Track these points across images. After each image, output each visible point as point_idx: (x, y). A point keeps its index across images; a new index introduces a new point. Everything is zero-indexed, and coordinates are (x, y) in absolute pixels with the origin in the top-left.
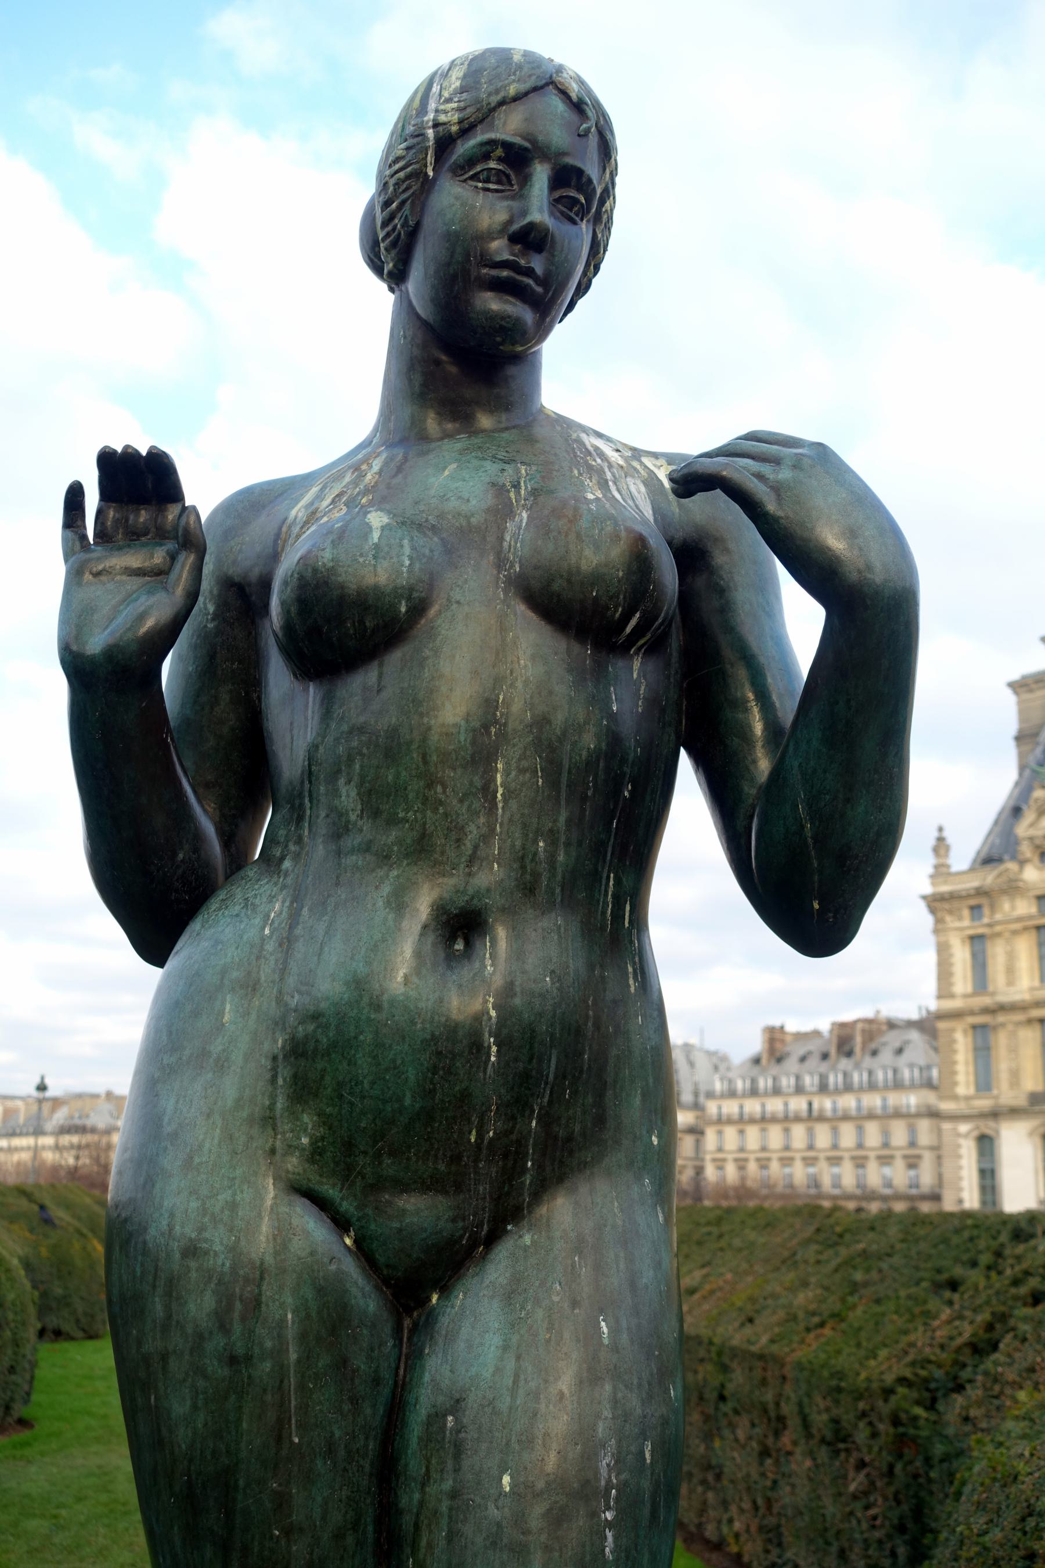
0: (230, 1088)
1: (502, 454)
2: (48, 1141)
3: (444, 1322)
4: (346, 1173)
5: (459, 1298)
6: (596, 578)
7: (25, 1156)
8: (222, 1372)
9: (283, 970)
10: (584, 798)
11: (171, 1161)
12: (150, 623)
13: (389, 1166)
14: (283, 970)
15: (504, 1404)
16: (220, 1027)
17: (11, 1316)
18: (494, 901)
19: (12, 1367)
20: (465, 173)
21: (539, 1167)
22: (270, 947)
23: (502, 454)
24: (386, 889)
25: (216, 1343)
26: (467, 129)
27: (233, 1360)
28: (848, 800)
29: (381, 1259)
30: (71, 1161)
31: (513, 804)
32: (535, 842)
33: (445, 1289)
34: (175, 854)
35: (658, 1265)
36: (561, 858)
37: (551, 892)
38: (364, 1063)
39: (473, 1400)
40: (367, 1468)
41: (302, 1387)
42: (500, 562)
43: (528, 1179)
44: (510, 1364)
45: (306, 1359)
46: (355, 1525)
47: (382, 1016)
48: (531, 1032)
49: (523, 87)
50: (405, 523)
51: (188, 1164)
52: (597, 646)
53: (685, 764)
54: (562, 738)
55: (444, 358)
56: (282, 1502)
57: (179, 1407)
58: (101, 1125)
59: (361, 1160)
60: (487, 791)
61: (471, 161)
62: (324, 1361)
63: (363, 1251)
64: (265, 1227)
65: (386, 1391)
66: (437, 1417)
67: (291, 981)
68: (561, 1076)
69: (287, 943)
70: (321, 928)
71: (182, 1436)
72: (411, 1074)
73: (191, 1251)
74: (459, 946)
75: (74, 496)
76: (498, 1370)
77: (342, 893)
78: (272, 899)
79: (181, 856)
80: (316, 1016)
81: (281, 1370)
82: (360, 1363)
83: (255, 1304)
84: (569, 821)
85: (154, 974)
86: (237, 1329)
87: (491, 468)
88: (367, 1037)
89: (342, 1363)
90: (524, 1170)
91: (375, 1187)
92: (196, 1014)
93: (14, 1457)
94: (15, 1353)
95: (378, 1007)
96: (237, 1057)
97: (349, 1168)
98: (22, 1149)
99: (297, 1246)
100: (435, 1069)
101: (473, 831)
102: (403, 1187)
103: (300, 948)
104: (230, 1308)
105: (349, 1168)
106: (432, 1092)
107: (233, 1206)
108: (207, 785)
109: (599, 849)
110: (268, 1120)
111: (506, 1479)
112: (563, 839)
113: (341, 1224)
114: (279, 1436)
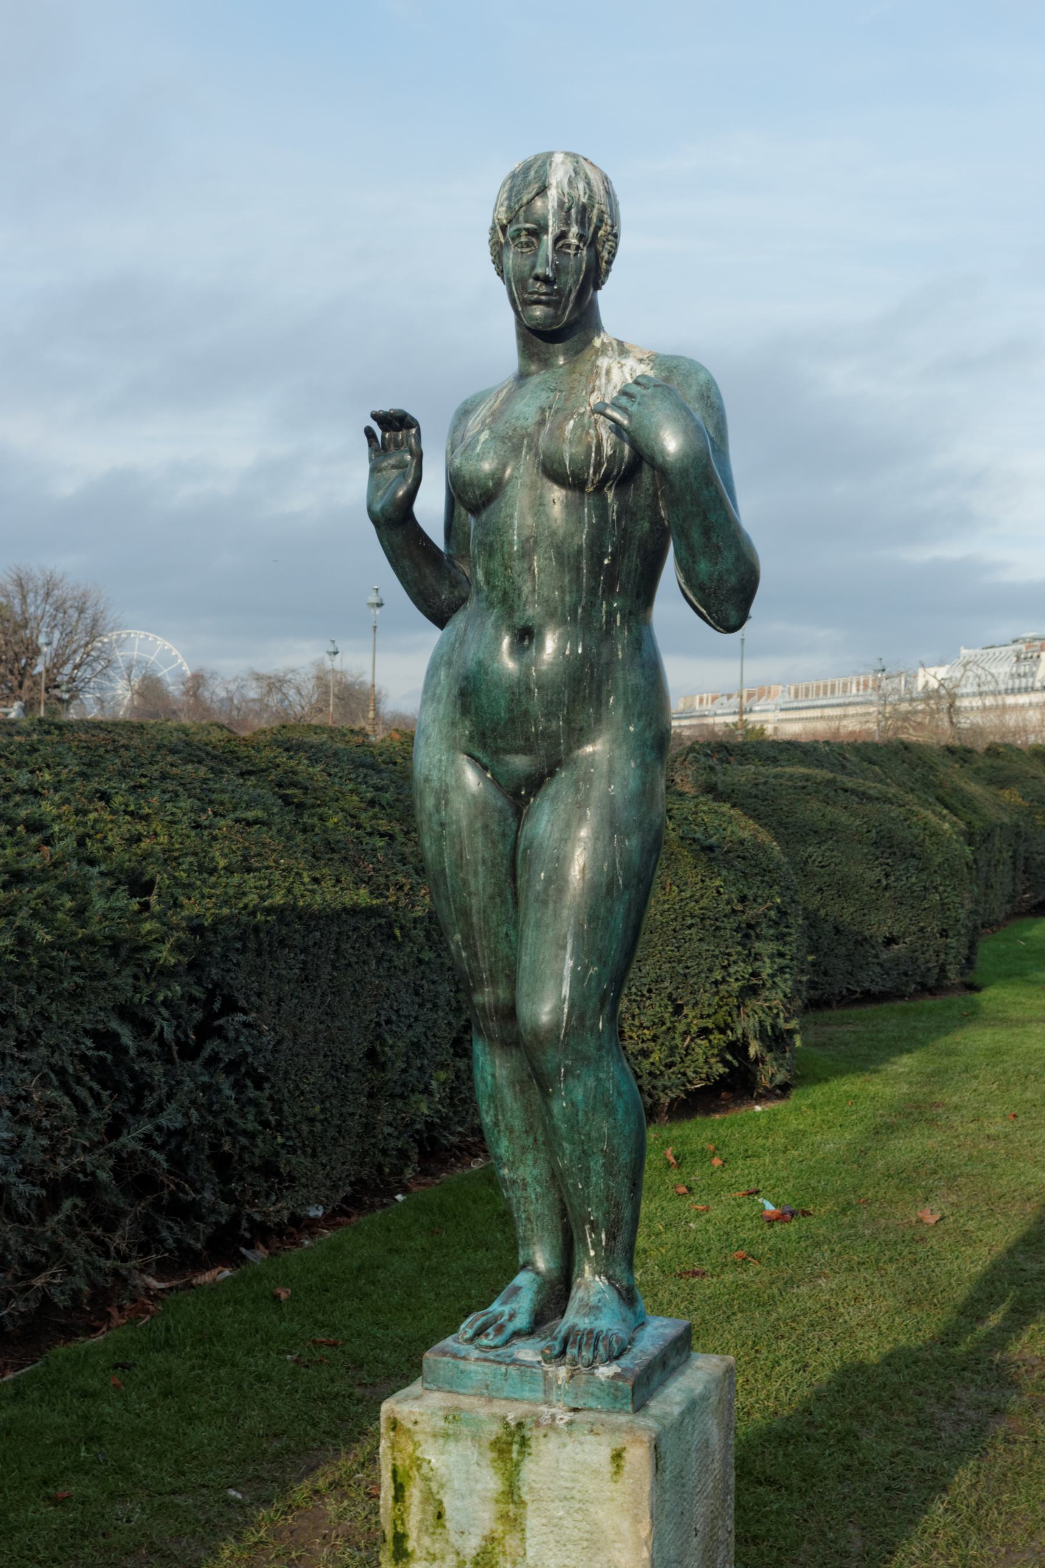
4: (484, 747)
8: (438, 829)
12: (401, 493)
13: (500, 743)
15: (545, 845)
25: (435, 818)
28: (694, 562)
31: (542, 575)
32: (553, 592)
34: (440, 597)
36: (567, 598)
38: (483, 698)
39: (536, 842)
40: (504, 871)
42: (536, 455)
43: (562, 748)
44: (549, 828)
45: (471, 824)
47: (489, 677)
59: (489, 741)
60: (530, 569)
65: (511, 840)
72: (503, 703)
75: (369, 433)
79: (443, 597)
84: (570, 581)
91: (496, 752)
95: (487, 674)
96: (444, 695)
97: (485, 744)
105: (485, 744)
106: (512, 710)
111: (542, 875)
112: (568, 589)
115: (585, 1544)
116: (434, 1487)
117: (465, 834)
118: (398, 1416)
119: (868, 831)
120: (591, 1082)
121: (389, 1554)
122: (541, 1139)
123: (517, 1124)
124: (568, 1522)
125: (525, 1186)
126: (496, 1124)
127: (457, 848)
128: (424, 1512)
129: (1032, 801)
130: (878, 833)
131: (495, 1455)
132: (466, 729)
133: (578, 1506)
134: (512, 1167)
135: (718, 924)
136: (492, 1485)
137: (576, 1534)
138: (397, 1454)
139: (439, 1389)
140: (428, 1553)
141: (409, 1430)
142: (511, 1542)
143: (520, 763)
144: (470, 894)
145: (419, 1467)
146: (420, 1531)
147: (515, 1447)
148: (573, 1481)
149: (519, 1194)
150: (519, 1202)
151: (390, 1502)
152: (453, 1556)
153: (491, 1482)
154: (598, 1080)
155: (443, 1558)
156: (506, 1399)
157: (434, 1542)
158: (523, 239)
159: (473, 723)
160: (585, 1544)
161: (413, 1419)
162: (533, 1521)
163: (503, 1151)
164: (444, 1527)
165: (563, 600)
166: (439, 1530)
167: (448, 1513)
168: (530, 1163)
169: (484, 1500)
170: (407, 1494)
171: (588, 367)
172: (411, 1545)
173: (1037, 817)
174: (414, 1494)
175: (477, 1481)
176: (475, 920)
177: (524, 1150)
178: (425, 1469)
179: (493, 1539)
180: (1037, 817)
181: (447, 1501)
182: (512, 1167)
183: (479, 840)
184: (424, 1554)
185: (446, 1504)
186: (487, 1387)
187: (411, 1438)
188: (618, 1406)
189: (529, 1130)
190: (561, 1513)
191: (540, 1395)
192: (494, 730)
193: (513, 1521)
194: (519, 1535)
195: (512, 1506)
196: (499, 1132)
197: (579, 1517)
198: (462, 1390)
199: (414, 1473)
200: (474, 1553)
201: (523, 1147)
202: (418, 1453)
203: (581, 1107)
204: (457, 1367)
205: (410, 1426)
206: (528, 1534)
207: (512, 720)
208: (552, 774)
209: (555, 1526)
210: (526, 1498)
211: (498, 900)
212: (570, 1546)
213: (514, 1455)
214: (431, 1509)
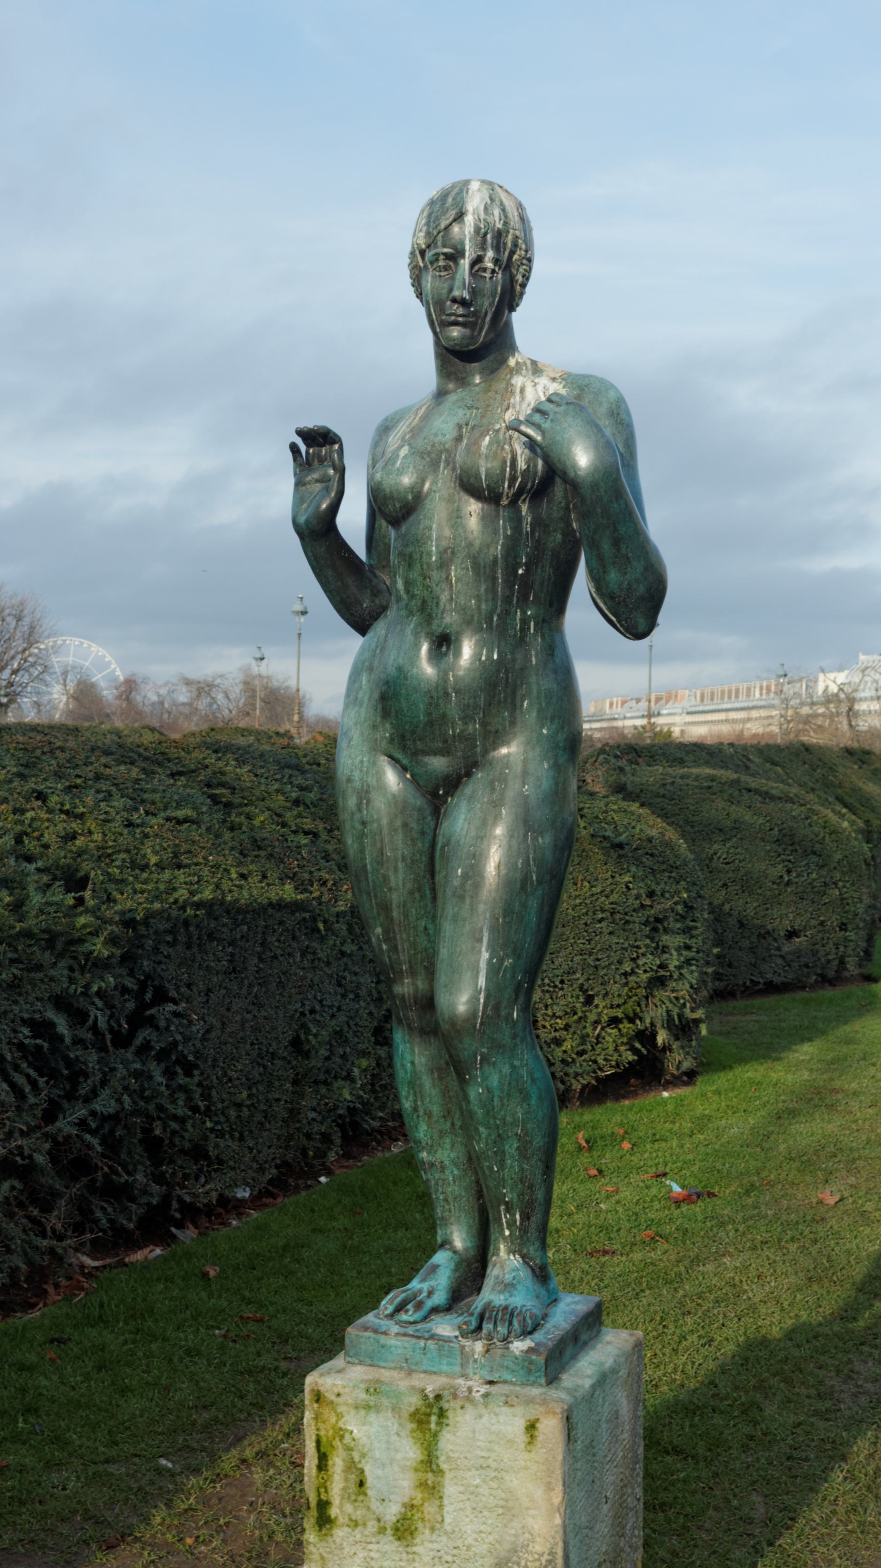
4: (404, 748)
12: (324, 506)
25: (357, 816)
36: (484, 607)
37: (480, 623)
38: (403, 701)
39: (453, 840)
40: (423, 867)
42: (454, 469)
43: (478, 749)
44: (466, 826)
45: (391, 822)
46: (419, 890)
54: (480, 552)
55: (333, 494)
60: (448, 578)
65: (429, 838)
75: (294, 448)
76: (462, 829)
84: (486, 590)
85: (355, 642)
90: (476, 746)
91: (415, 754)
95: (406, 679)
96: (366, 699)
100: (431, 704)
102: (426, 753)
106: (431, 714)
115: (500, 1511)
116: (356, 1456)
118: (322, 1389)
120: (506, 1070)
121: (313, 1521)
122: (458, 1124)
123: (435, 1109)
124: (484, 1490)
125: (443, 1169)
126: (415, 1109)
128: (346, 1480)
130: (780, 831)
131: (414, 1426)
132: (386, 731)
133: (493, 1474)
134: (431, 1150)
135: (627, 918)
139: (361, 1363)
140: (351, 1520)
141: (332, 1402)
142: (430, 1509)
143: (438, 764)
145: (342, 1437)
147: (434, 1418)
148: (489, 1450)
149: (437, 1176)
150: (437, 1184)
152: (375, 1523)
155: (365, 1524)
156: (425, 1372)
157: (356, 1508)
159: (393, 726)
160: (500, 1511)
161: (336, 1391)
162: (450, 1489)
163: (422, 1135)
164: (365, 1494)
166: (361, 1498)
167: (370, 1481)
168: (448, 1146)
170: (330, 1463)
171: (503, 385)
172: (334, 1512)
174: (337, 1463)
175: (397, 1451)
176: (395, 914)
177: (442, 1134)
178: (347, 1439)
182: (431, 1150)
184: (346, 1520)
185: (367, 1473)
186: (407, 1360)
188: (532, 1378)
189: (447, 1115)
190: (477, 1481)
192: (413, 732)
194: (437, 1502)
195: (430, 1475)
196: (418, 1117)
197: (494, 1485)
198: (382, 1364)
199: (337, 1443)
200: (394, 1519)
202: (341, 1424)
203: (497, 1093)
204: (378, 1342)
205: (333, 1398)
206: (446, 1501)
208: (469, 774)
210: (444, 1466)
212: (486, 1513)
213: (433, 1426)
214: (353, 1477)
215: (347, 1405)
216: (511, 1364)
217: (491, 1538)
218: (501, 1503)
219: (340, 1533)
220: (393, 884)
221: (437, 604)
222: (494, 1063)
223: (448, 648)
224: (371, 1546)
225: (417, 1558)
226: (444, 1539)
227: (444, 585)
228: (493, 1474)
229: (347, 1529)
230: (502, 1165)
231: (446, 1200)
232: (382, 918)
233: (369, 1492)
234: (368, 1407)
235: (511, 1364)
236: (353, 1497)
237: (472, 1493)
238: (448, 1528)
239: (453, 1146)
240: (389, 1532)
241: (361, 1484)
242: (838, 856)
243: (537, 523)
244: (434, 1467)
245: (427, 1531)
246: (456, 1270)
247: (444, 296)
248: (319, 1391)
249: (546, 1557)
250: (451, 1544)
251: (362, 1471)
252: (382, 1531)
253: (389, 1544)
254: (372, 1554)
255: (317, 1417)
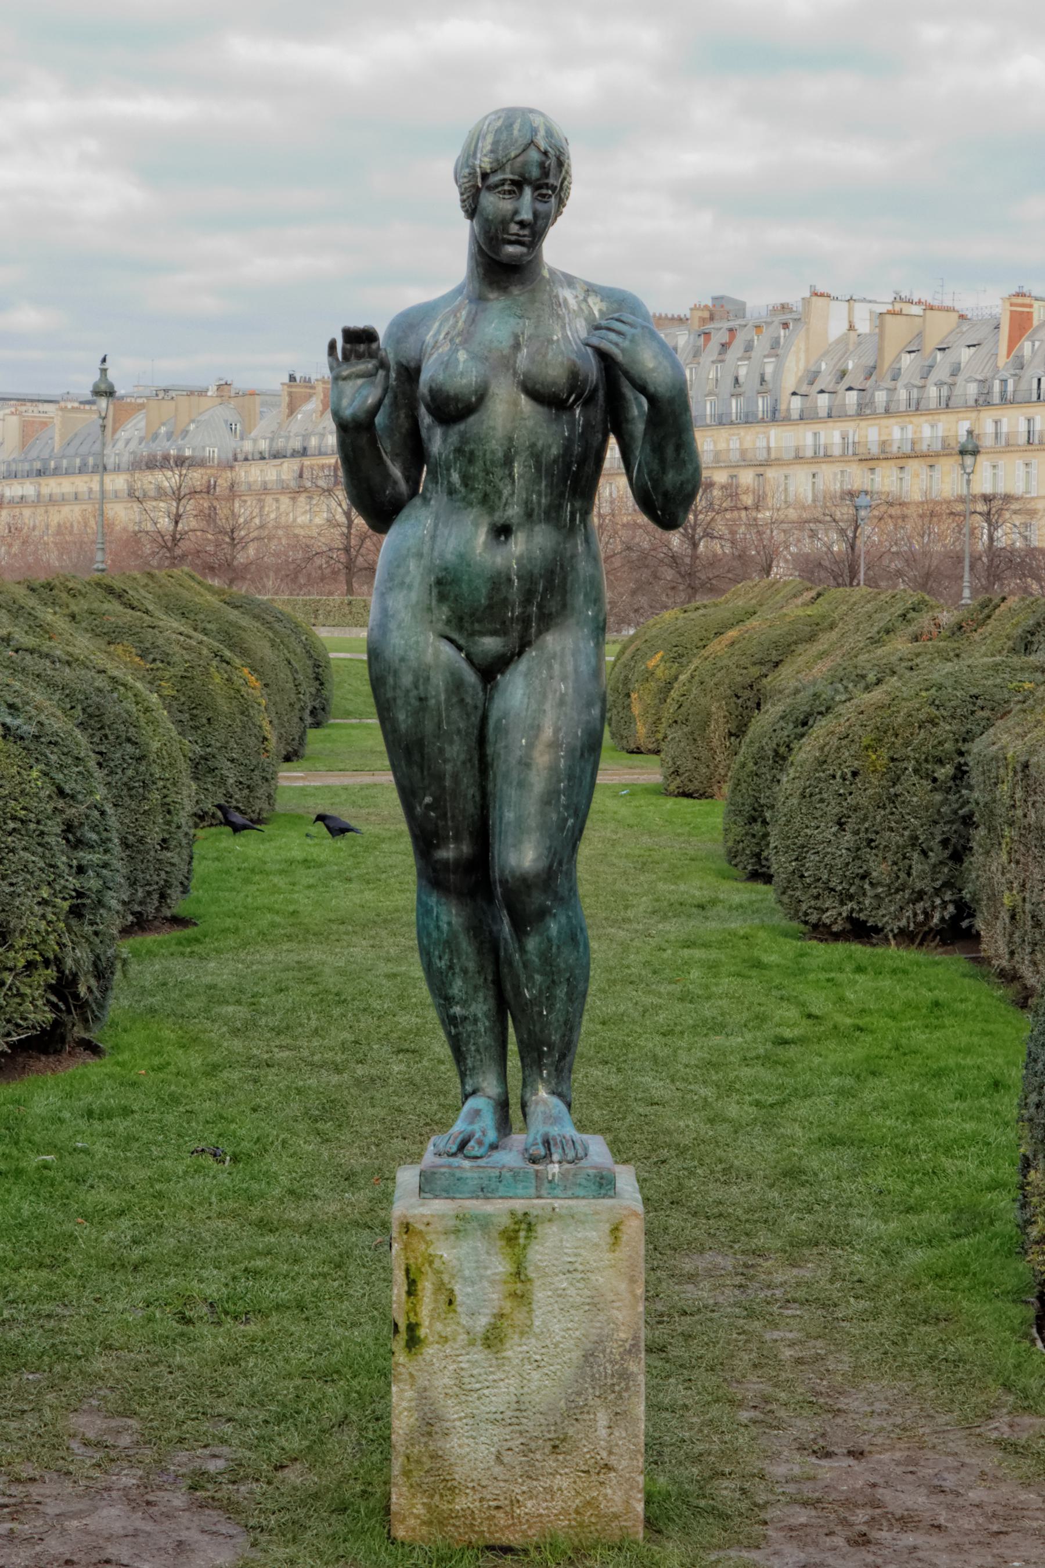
0: (414, 596)
1: (519, 312)
2: (117, 482)
3: (501, 686)
4: (460, 628)
5: (508, 676)
6: (554, 384)
7: (71, 513)
8: (416, 703)
9: (432, 549)
10: (553, 475)
11: (392, 625)
12: (370, 401)
13: (477, 626)
14: (432, 549)
16: (408, 572)
17: (157, 771)
18: (515, 521)
19: (164, 840)
20: (368, 786)
21: (538, 625)
22: (427, 539)
23: (519, 312)
24: (472, 517)
25: (414, 693)
26: (494, 171)
27: (421, 699)
29: (476, 661)
30: (165, 523)
33: (503, 673)
35: (589, 663)
36: (543, 501)
38: (464, 586)
41: (446, 709)
42: (515, 374)
43: (533, 630)
44: (526, 700)
46: (470, 760)
48: (531, 574)
49: (518, 152)
50: (474, 357)
51: (399, 627)
52: (557, 409)
53: (612, 441)
54: (541, 452)
56: (441, 751)
57: (401, 716)
58: (213, 452)
60: (511, 476)
61: (496, 186)
62: (454, 700)
63: (469, 658)
64: (430, 650)
65: (480, 712)
66: (499, 720)
67: (436, 554)
68: (545, 589)
69: (433, 537)
70: (446, 532)
71: (403, 727)
73: (402, 660)
74: (503, 538)
75: (332, 346)
77: (454, 517)
78: (427, 518)
80: (446, 569)
81: (438, 703)
82: (469, 700)
83: (428, 679)
86: (421, 687)
87: (513, 321)
88: (466, 577)
89: (462, 701)
91: (472, 634)
92: (398, 566)
93: (183, 954)
94: (168, 823)
95: (469, 566)
96: (416, 584)
98: (63, 500)
99: (443, 657)
101: (506, 492)
102: (483, 634)
103: (439, 541)
104: (418, 680)
107: (417, 643)
108: (397, 455)
109: (562, 495)
110: (430, 609)
113: (460, 648)
114: (439, 726)
115: (587, 1308)
116: (446, 1278)
117: (443, 706)
118: (411, 1220)
119: (72, 708)
120: (563, 920)
121: (403, 1343)
122: (490, 978)
123: (471, 966)
124: (572, 1291)
125: (476, 1020)
126: (451, 967)
127: (436, 720)
128: (436, 1301)
129: (154, 660)
130: (84, 710)
131: (503, 1243)
132: (444, 612)
133: (579, 1276)
134: (465, 1003)
135: (41, 827)
136: (501, 1269)
137: (578, 1299)
138: (410, 1254)
139: (436, 1197)
140: (441, 1337)
141: (421, 1232)
142: (520, 1317)
143: (490, 644)
144: (445, 761)
145: (431, 1263)
146: (432, 1318)
147: (522, 1234)
148: (576, 1255)
149: (469, 1029)
150: (469, 1036)
151: (404, 1296)
152: (464, 1336)
153: (500, 1266)
154: (568, 917)
155: (454, 1339)
156: (501, 1198)
157: (445, 1325)
158: (506, 187)
159: (452, 610)
160: (587, 1308)
161: (425, 1220)
162: (540, 1295)
163: (456, 991)
164: (455, 1311)
165: (539, 503)
166: (451, 1315)
167: (459, 1298)
168: (481, 999)
169: (492, 1282)
170: (420, 1287)
171: (546, 297)
172: (422, 1332)
173: (163, 683)
174: (426, 1286)
175: (486, 1268)
176: (447, 784)
177: (476, 988)
178: (437, 1264)
179: (502, 1315)
180: (163, 683)
181: (457, 1288)
182: (465, 1003)
183: (455, 714)
184: (436, 1337)
185: (456, 1292)
186: (482, 1190)
187: (423, 1237)
188: (603, 1192)
189: (481, 970)
190: (565, 1285)
191: (532, 1191)
192: (472, 615)
193: (521, 1298)
194: (526, 1309)
195: (519, 1285)
196: (454, 974)
197: (580, 1285)
198: (458, 1195)
199: (426, 1268)
200: (483, 1330)
201: (475, 987)
202: (431, 1251)
203: (555, 942)
204: (453, 1175)
205: (422, 1227)
206: (534, 1306)
207: (490, 607)
208: (520, 654)
209: (560, 1296)
210: (532, 1275)
211: (468, 765)
212: (572, 1312)
213: (522, 1241)
214: (443, 1298)
215: (437, 1233)
216: (584, 1182)
217: (578, 1333)
218: (588, 1300)
219: (429, 1351)
220: (448, 755)
221: (500, 498)
222: (555, 915)
223: (507, 538)
224: (460, 1358)
225: (506, 1362)
226: (533, 1340)
227: (507, 481)
228: (579, 1276)
229: (436, 1346)
230: (551, 1008)
231: (478, 1051)
232: (433, 788)
233: (459, 1309)
234: (457, 1231)
235: (584, 1182)
236: (443, 1316)
237: (560, 1296)
238: (537, 1330)
239: (485, 999)
240: (479, 1342)
241: (450, 1303)
242: (155, 745)
243: (587, 425)
244: (522, 1277)
245: (516, 1337)
246: (495, 1113)
247: (509, 217)
248: (408, 1224)
249: (630, 1342)
250: (540, 1344)
251: (452, 1291)
252: (472, 1343)
253: (479, 1354)
254: (462, 1365)
255: (406, 1247)
